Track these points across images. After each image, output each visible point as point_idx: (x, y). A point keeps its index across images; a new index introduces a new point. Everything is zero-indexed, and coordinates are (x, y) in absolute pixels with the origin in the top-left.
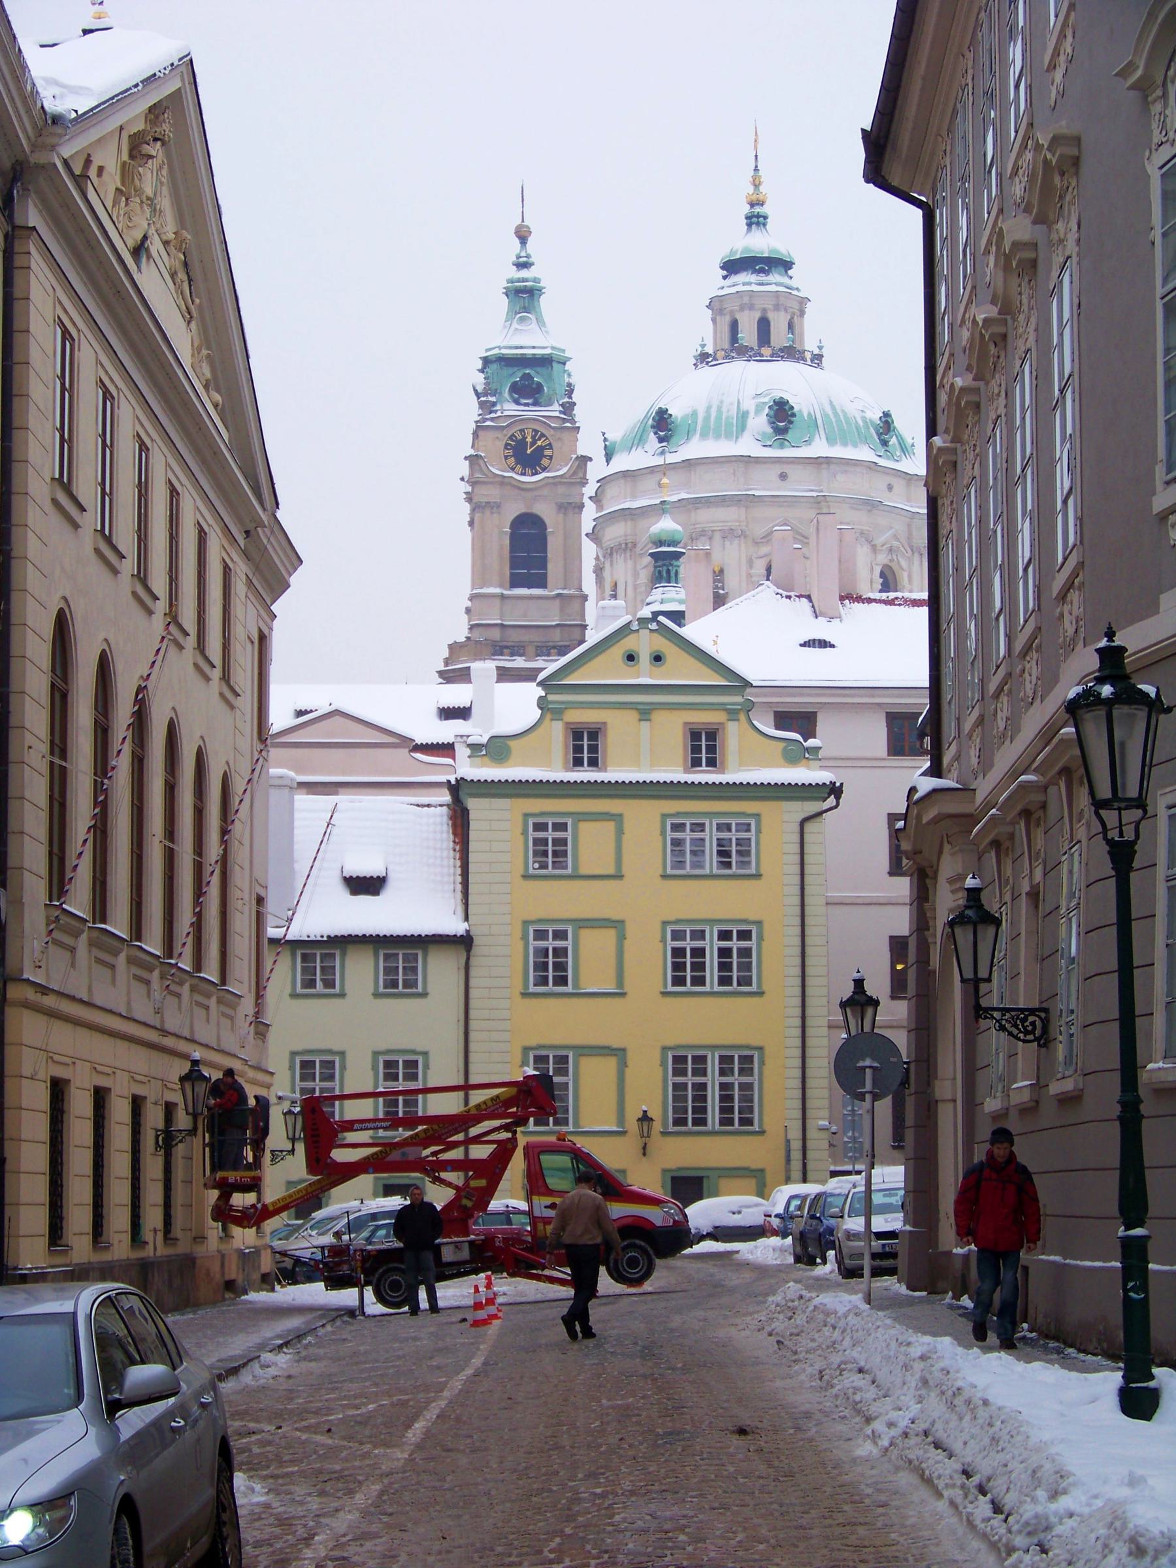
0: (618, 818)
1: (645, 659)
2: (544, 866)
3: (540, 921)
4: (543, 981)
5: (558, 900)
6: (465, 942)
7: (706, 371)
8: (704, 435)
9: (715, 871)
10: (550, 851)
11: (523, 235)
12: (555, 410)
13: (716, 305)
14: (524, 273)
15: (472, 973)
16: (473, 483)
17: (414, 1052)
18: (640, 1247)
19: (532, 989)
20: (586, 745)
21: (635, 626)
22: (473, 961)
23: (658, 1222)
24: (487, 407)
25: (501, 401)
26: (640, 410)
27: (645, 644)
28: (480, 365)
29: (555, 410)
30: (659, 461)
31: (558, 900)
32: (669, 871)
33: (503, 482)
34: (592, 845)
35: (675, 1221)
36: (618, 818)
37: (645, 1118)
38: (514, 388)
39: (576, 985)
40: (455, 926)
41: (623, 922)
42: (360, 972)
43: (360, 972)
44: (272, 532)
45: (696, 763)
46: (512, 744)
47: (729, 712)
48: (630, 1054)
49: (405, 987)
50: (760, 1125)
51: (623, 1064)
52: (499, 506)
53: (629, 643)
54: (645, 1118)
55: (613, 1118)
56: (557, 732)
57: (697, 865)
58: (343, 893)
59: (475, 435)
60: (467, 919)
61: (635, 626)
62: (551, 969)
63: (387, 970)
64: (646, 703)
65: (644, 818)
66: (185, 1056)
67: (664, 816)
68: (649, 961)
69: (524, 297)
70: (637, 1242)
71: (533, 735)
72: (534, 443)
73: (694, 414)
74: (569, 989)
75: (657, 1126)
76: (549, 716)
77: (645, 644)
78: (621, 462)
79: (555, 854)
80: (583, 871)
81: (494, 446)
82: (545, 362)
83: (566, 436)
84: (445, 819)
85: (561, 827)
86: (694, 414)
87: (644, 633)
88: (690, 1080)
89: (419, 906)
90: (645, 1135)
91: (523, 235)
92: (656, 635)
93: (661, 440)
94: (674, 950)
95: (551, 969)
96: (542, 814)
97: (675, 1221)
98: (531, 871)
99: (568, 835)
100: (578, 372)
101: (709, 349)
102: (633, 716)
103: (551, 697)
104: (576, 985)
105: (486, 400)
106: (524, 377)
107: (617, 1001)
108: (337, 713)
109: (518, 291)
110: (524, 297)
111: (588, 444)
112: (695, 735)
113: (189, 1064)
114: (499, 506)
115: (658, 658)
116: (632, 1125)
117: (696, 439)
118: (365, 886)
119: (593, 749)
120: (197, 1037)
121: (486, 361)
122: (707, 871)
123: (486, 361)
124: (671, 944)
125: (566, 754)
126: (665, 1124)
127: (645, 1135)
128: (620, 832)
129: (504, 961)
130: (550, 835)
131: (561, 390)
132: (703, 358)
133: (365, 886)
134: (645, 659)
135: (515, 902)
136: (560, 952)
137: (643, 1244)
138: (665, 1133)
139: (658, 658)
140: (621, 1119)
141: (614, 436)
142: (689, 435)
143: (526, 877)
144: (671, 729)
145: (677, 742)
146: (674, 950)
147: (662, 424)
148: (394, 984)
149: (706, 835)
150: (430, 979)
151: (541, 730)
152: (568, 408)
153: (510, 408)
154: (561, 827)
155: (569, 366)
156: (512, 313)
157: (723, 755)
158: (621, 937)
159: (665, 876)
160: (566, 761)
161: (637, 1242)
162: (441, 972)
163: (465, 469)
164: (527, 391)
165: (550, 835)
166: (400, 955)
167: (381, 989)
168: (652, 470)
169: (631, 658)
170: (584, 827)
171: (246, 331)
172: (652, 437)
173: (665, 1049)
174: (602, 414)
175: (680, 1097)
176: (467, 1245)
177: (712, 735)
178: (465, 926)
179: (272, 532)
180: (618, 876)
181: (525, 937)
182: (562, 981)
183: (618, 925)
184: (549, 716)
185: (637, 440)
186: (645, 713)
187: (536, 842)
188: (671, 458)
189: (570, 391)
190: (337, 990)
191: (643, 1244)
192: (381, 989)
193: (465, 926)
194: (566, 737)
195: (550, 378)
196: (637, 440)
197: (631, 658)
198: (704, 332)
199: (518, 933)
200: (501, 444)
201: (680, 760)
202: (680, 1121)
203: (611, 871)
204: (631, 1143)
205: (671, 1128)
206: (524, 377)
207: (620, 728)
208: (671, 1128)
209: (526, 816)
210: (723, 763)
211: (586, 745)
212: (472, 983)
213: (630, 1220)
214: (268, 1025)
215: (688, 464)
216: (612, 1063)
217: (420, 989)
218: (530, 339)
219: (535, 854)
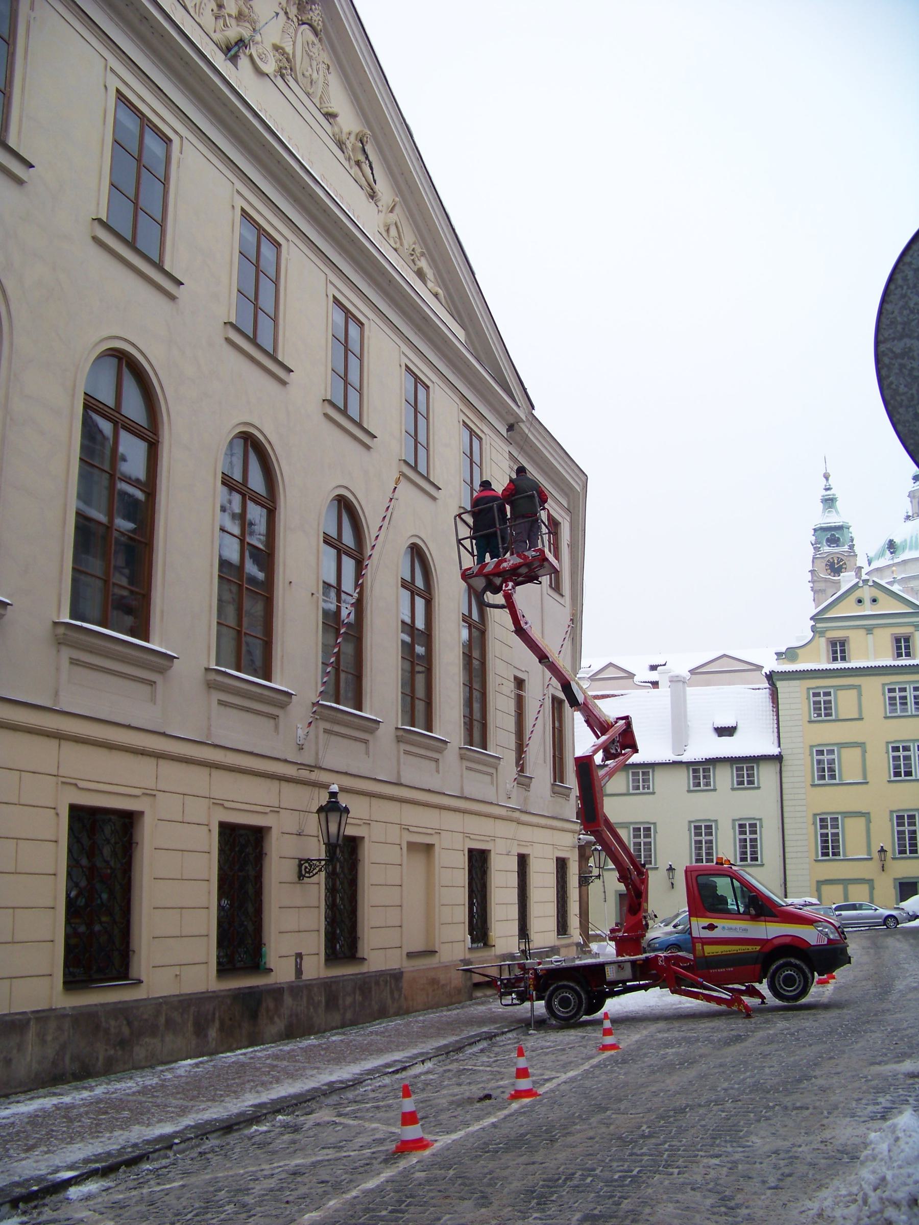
0: (858, 687)
1: (867, 601)
2: (819, 715)
3: (819, 745)
4: (822, 777)
5: (828, 733)
6: (778, 758)
7: (909, 523)
8: (911, 549)
9: (914, 713)
10: (823, 709)
11: (827, 477)
12: (846, 548)
13: (911, 495)
14: (829, 492)
15: (784, 775)
16: (812, 581)
17: (754, 819)
18: (796, 966)
19: (817, 782)
20: (839, 649)
21: (861, 584)
22: (783, 769)
23: (813, 942)
24: (817, 549)
25: (823, 546)
26: (882, 541)
27: (866, 593)
28: (813, 532)
29: (846, 548)
30: (891, 562)
31: (828, 733)
32: (888, 715)
33: (826, 580)
34: (845, 703)
35: (829, 940)
36: (858, 687)
37: (882, 850)
38: (828, 540)
39: (840, 779)
40: (774, 750)
41: (864, 743)
42: (724, 777)
43: (724, 777)
44: (531, 424)
45: (899, 655)
46: (798, 651)
47: (915, 626)
48: (872, 815)
49: (748, 784)
50: (714, 786)
51: (869, 821)
52: (825, 590)
53: (858, 594)
54: (882, 850)
55: (865, 850)
56: (822, 642)
57: (906, 710)
58: (714, 736)
59: (813, 562)
60: (779, 746)
61: (861, 584)
62: (826, 772)
63: (738, 776)
64: (869, 625)
65: (873, 687)
66: (326, 786)
67: (884, 685)
68: (880, 763)
69: (829, 502)
70: (793, 960)
71: (808, 647)
72: (838, 563)
73: (905, 541)
74: (837, 781)
75: (889, 855)
76: (817, 635)
77: (866, 593)
78: (875, 565)
79: (825, 709)
80: (841, 717)
81: (821, 566)
82: (840, 528)
83: (851, 558)
84: (768, 695)
85: (828, 694)
86: (905, 541)
87: (866, 587)
88: (906, 828)
89: (754, 741)
90: (883, 861)
91: (827, 477)
92: (872, 588)
93: (892, 553)
94: (894, 757)
95: (826, 772)
96: (818, 687)
97: (829, 940)
98: (813, 719)
99: (832, 698)
100: (854, 532)
101: (910, 514)
102: (862, 632)
103: (818, 625)
104: (840, 779)
105: (816, 547)
106: (832, 535)
107: (864, 786)
108: (725, 656)
109: (827, 500)
110: (829, 502)
111: (861, 561)
112: (898, 640)
113: (328, 796)
114: (825, 590)
115: (874, 601)
116: (875, 855)
117: (907, 551)
118: (725, 731)
119: (843, 651)
120: (403, 781)
121: (815, 530)
122: (909, 713)
123: (815, 530)
124: (892, 754)
125: (828, 655)
126: (894, 853)
127: (883, 861)
128: (860, 695)
129: (799, 768)
130: (822, 699)
131: (848, 540)
132: (908, 518)
133: (725, 731)
134: (867, 601)
135: (802, 736)
136: (831, 762)
137: (798, 962)
138: (893, 859)
139: (874, 601)
140: (869, 852)
141: (871, 555)
142: (904, 550)
143: (810, 722)
144: (884, 638)
145: (888, 645)
146: (894, 757)
147: (892, 546)
148: (742, 783)
149: (907, 694)
150: (761, 778)
151: (813, 643)
152: (852, 547)
153: (826, 549)
154: (827, 694)
155: (851, 530)
156: (825, 509)
157: (914, 650)
158: (864, 752)
159: (886, 717)
160: (828, 658)
161: (793, 960)
162: (766, 775)
163: (809, 577)
164: (833, 541)
165: (822, 699)
166: (745, 767)
167: (735, 786)
168: (889, 566)
169: (860, 601)
170: (841, 693)
171: (457, 231)
172: (888, 552)
173: (892, 812)
174: (866, 545)
175: (901, 837)
176: (629, 964)
177: (907, 640)
178: (779, 750)
179: (531, 424)
180: (861, 719)
181: (811, 754)
182: (833, 777)
183: (861, 745)
184: (817, 635)
185: (881, 554)
186: (869, 630)
187: (815, 703)
188: (896, 561)
189: (852, 540)
190: (712, 787)
191: (798, 962)
192: (735, 786)
193: (779, 750)
194: (827, 645)
195: (843, 535)
196: (881, 554)
197: (860, 601)
198: (907, 506)
199: (808, 752)
200: (824, 565)
201: (890, 654)
202: (902, 852)
203: (856, 716)
204: (875, 865)
205: (897, 856)
206: (832, 535)
207: (856, 639)
208: (897, 856)
209: (808, 689)
210: (914, 655)
211: (839, 649)
212: (784, 779)
213: (788, 940)
214: (531, 778)
215: (904, 562)
216: (862, 820)
217: (756, 785)
218: (833, 519)
219: (815, 709)
